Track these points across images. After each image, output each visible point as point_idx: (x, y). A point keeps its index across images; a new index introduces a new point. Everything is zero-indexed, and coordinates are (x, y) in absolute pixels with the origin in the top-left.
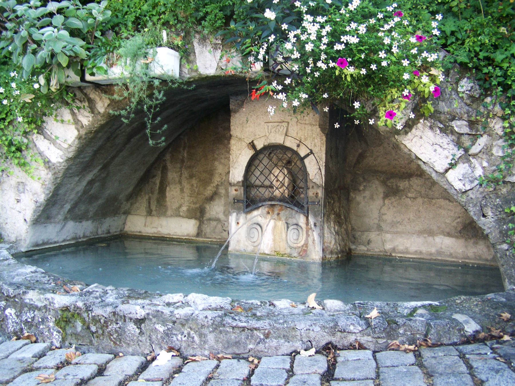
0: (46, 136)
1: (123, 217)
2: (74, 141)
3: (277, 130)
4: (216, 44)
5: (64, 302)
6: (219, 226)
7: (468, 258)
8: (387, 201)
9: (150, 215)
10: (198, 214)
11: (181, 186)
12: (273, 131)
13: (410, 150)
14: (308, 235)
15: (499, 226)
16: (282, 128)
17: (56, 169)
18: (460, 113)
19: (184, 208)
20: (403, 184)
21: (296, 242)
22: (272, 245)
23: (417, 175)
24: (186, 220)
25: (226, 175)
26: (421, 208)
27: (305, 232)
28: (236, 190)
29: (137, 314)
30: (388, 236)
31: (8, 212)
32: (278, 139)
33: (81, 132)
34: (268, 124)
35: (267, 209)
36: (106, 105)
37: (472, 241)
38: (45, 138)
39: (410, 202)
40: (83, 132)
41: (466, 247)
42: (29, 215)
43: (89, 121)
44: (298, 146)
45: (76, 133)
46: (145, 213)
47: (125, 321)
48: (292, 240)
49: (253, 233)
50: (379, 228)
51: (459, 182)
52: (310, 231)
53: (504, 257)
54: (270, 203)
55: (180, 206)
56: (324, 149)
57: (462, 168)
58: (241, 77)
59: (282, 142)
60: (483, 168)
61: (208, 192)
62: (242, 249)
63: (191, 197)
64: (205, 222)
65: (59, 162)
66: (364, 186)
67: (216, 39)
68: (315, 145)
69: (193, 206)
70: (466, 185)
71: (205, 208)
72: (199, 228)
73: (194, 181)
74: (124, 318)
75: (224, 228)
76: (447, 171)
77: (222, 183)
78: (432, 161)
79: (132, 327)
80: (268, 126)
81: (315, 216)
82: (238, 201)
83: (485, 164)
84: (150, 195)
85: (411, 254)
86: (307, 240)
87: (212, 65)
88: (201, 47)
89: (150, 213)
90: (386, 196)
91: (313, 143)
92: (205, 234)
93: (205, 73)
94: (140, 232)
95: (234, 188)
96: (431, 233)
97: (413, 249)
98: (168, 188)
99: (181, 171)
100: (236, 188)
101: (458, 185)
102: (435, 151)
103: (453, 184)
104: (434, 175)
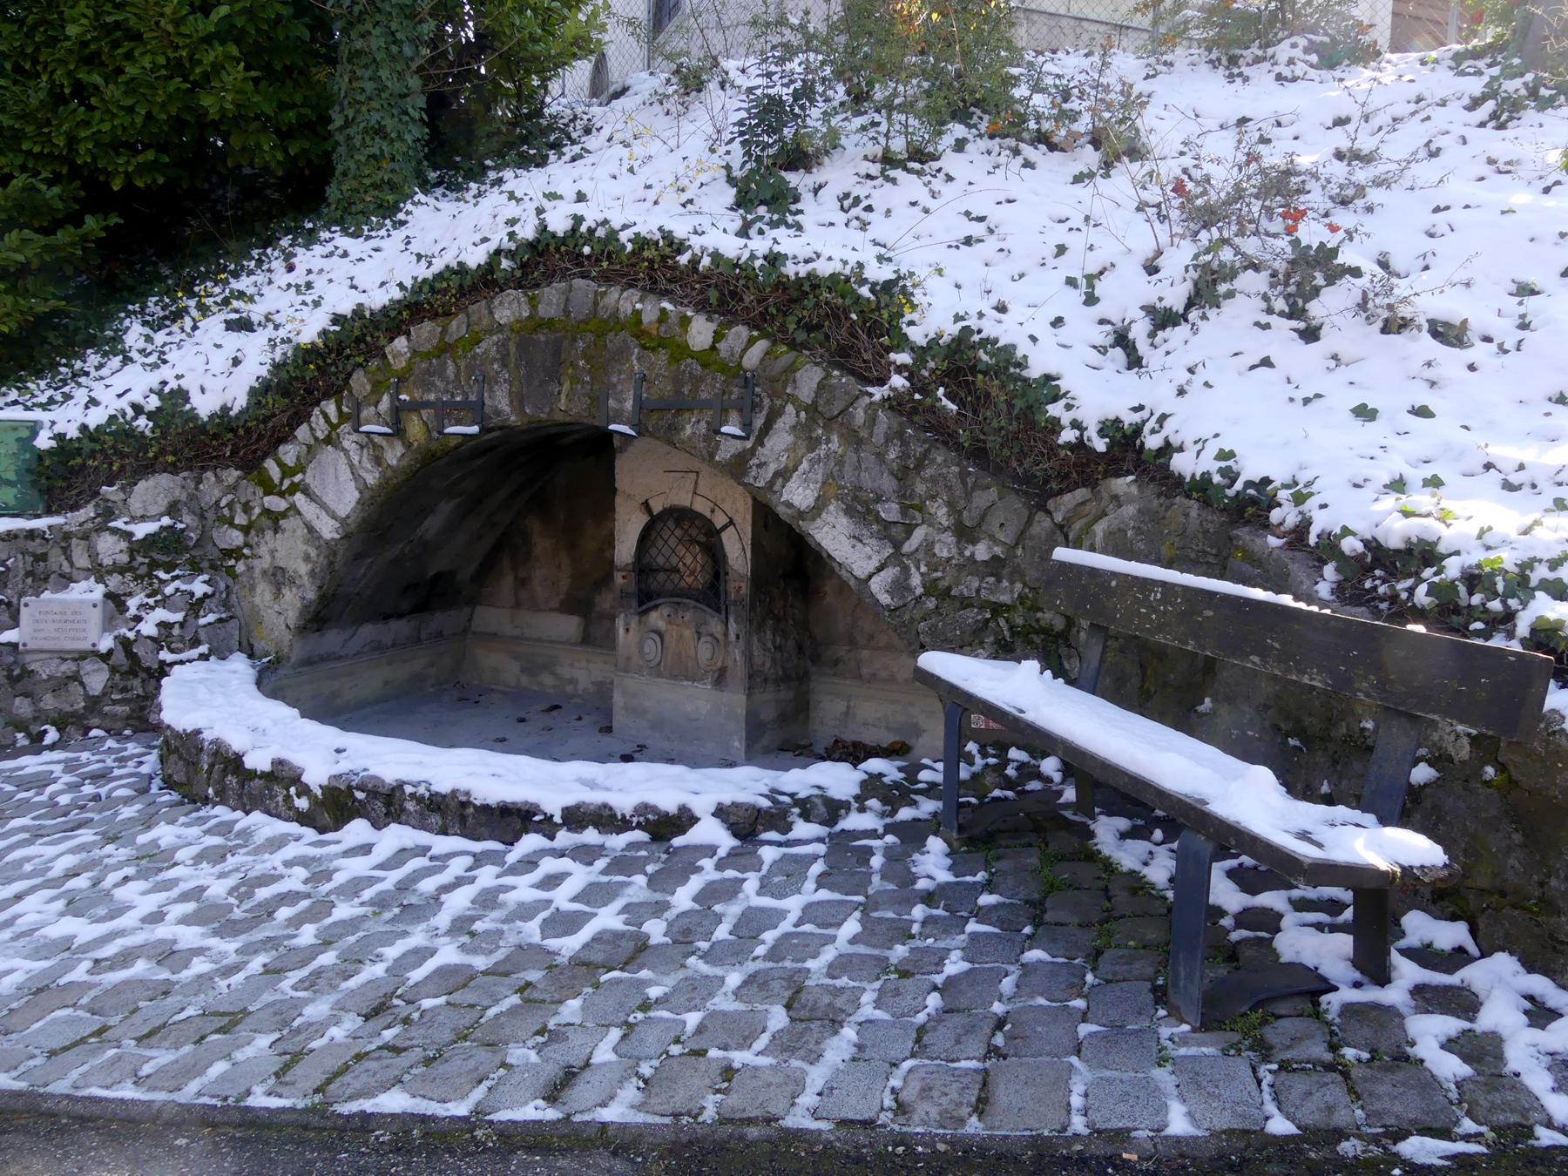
1: (467, 610)
30: (865, 653)
32: (683, 499)
40: (367, 494)
42: (292, 617)
44: (713, 511)
45: (357, 495)
50: (852, 642)
56: (749, 518)
59: (687, 504)
60: (922, 574)
76: (870, 576)
104: (852, 582)
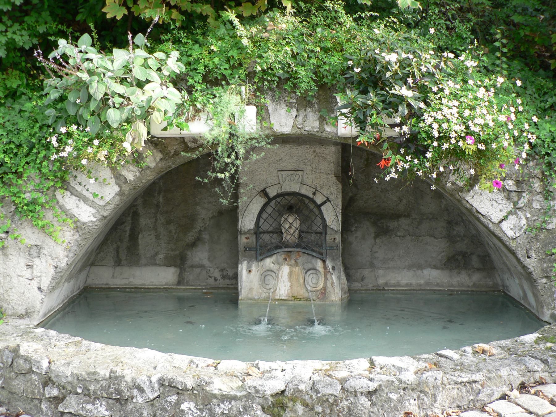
0: (73, 191)
2: (114, 197)
3: (292, 179)
4: (290, 103)
5: (279, 388)
6: (204, 272)
7: (453, 286)
8: (378, 241)
9: (119, 265)
10: (178, 262)
11: (156, 232)
12: (287, 179)
13: (472, 206)
14: (326, 279)
15: (541, 265)
16: (298, 176)
17: (86, 229)
18: (510, 174)
19: (161, 256)
20: (393, 224)
21: (315, 286)
22: (289, 291)
23: (405, 216)
24: (165, 268)
25: (209, 220)
26: (410, 245)
27: (323, 276)
28: (247, 238)
29: (369, 387)
30: (381, 272)
31: (13, 280)
33: (123, 188)
34: (282, 173)
35: (283, 256)
36: (158, 159)
37: (456, 271)
38: (72, 194)
39: (399, 240)
40: (126, 188)
41: (451, 277)
43: (134, 176)
44: (314, 194)
46: (113, 264)
47: (356, 396)
48: (311, 284)
49: (269, 280)
51: (511, 231)
52: (329, 275)
53: (544, 289)
54: (286, 249)
55: (156, 254)
57: (512, 219)
58: (318, 136)
60: (527, 218)
61: (190, 238)
62: (256, 297)
63: (169, 243)
64: (187, 269)
65: (92, 222)
66: (356, 227)
67: (291, 98)
68: (331, 193)
69: (172, 253)
70: (517, 233)
71: (186, 254)
72: (180, 275)
73: (172, 227)
74: (355, 394)
75: (209, 274)
76: (501, 222)
77: (205, 228)
78: (489, 214)
79: (364, 401)
80: (282, 175)
81: (333, 260)
82: (251, 249)
83: (529, 216)
84: (119, 243)
85: (403, 286)
86: (325, 283)
87: (288, 123)
88: (274, 104)
89: (118, 263)
90: (377, 236)
91: (329, 191)
92: (187, 282)
93: (279, 131)
94: (106, 284)
95: (243, 237)
96: (420, 267)
97: (404, 282)
98: (140, 236)
99: (156, 217)
100: (248, 236)
101: (510, 233)
102: (492, 205)
103: (506, 232)
